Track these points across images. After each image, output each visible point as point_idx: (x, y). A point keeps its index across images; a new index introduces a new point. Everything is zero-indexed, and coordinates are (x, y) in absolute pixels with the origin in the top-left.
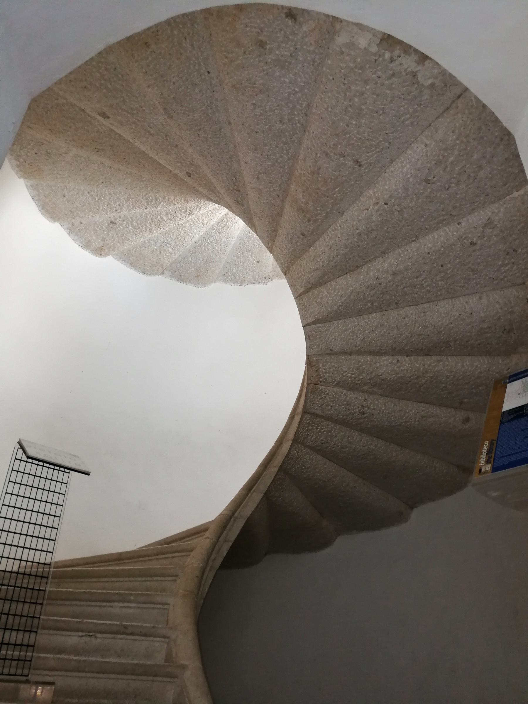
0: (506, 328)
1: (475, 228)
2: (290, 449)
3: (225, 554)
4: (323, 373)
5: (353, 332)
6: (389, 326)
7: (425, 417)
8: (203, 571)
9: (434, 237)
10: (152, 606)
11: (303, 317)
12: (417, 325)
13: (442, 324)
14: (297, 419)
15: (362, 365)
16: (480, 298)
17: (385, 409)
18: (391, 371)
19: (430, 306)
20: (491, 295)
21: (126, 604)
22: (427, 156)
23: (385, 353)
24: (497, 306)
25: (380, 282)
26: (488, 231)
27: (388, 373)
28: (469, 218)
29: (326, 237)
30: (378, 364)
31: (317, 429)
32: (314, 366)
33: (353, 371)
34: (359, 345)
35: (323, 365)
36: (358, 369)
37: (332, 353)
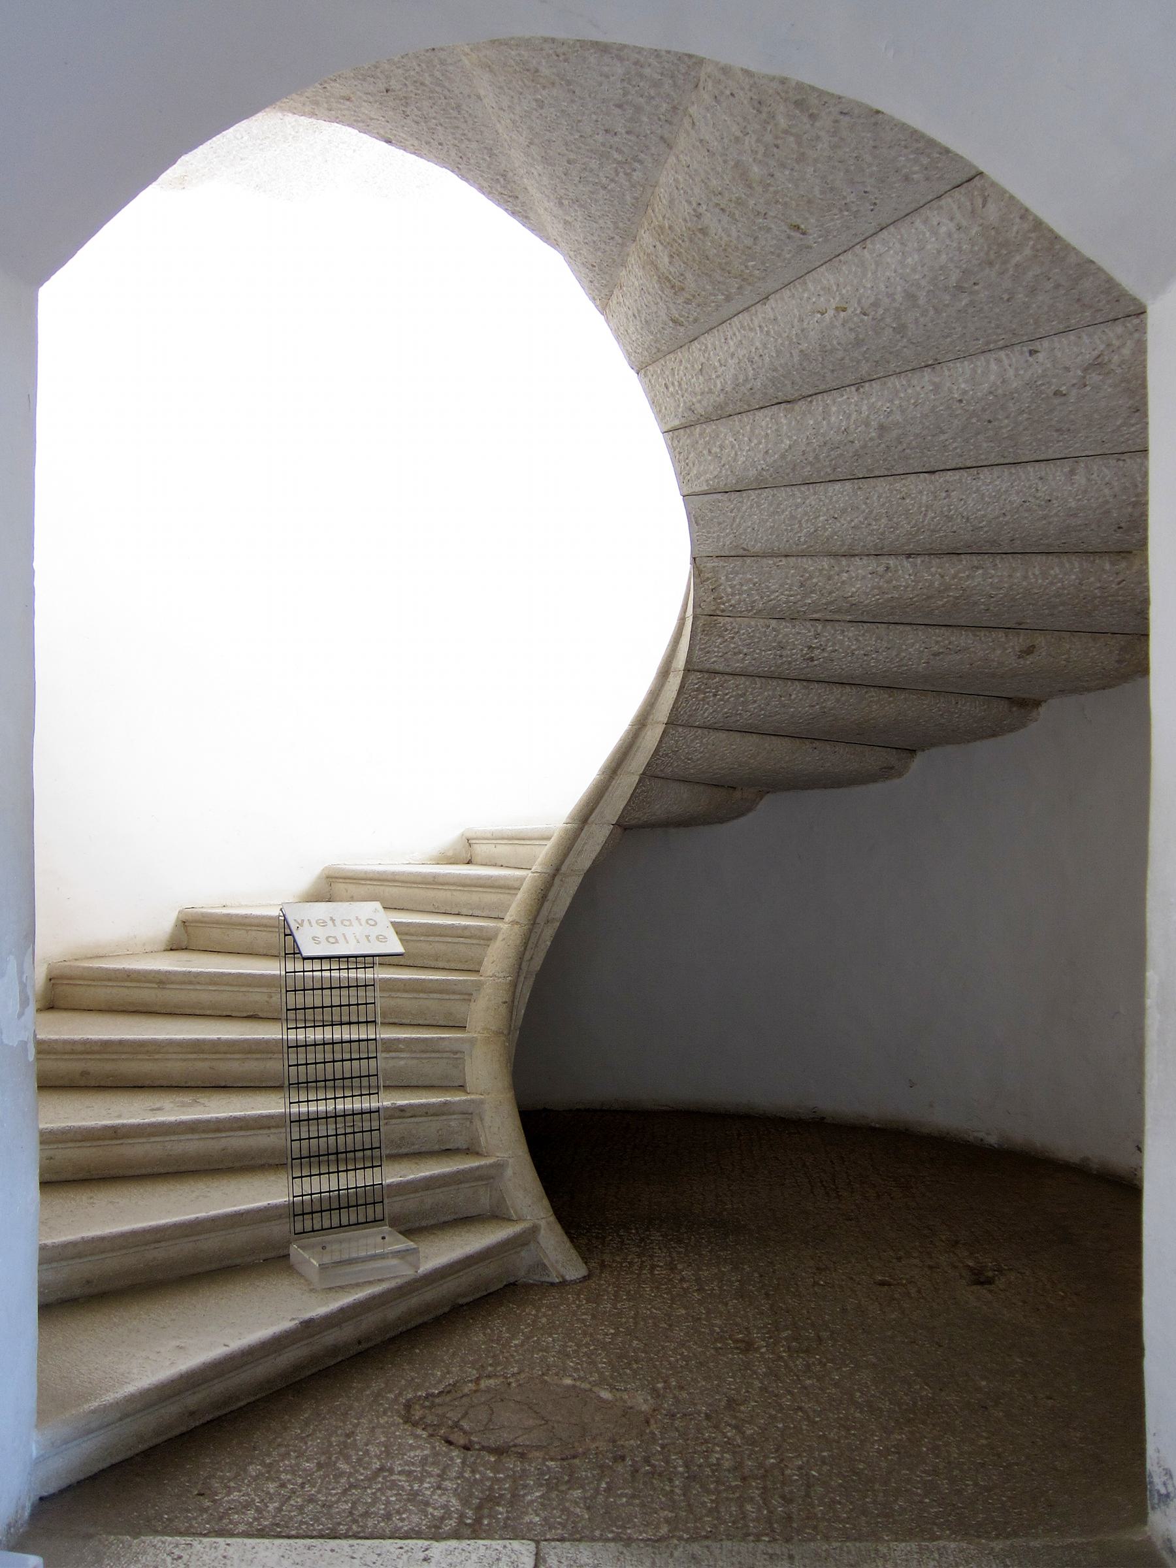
0: (1122, 525)
1: (1067, 369)
2: (660, 741)
3: (549, 943)
4: (728, 595)
5: (792, 517)
6: (871, 512)
7: (939, 654)
8: (514, 985)
9: (974, 371)
10: (437, 1055)
11: (683, 476)
12: (931, 514)
13: (984, 516)
14: (674, 682)
15: (811, 577)
16: (1072, 472)
17: (858, 648)
18: (873, 588)
19: (960, 479)
20: (1095, 468)
21: (393, 1054)
22: (960, 249)
23: (860, 555)
24: (1107, 491)
25: (851, 438)
26: (1094, 378)
27: (867, 594)
28: (1057, 345)
29: (729, 334)
30: (845, 576)
31: (715, 695)
32: (708, 579)
33: (791, 589)
34: (806, 542)
35: (727, 579)
36: (802, 585)
37: (744, 555)
